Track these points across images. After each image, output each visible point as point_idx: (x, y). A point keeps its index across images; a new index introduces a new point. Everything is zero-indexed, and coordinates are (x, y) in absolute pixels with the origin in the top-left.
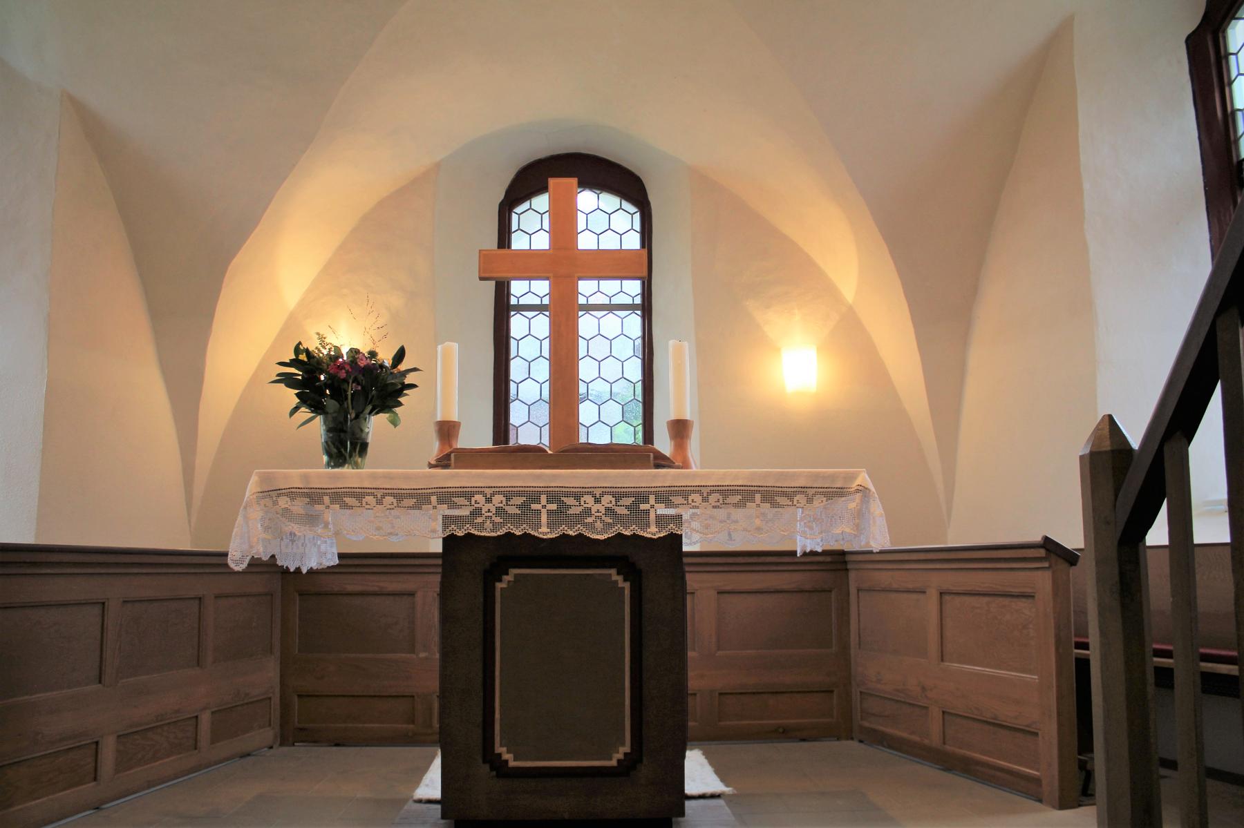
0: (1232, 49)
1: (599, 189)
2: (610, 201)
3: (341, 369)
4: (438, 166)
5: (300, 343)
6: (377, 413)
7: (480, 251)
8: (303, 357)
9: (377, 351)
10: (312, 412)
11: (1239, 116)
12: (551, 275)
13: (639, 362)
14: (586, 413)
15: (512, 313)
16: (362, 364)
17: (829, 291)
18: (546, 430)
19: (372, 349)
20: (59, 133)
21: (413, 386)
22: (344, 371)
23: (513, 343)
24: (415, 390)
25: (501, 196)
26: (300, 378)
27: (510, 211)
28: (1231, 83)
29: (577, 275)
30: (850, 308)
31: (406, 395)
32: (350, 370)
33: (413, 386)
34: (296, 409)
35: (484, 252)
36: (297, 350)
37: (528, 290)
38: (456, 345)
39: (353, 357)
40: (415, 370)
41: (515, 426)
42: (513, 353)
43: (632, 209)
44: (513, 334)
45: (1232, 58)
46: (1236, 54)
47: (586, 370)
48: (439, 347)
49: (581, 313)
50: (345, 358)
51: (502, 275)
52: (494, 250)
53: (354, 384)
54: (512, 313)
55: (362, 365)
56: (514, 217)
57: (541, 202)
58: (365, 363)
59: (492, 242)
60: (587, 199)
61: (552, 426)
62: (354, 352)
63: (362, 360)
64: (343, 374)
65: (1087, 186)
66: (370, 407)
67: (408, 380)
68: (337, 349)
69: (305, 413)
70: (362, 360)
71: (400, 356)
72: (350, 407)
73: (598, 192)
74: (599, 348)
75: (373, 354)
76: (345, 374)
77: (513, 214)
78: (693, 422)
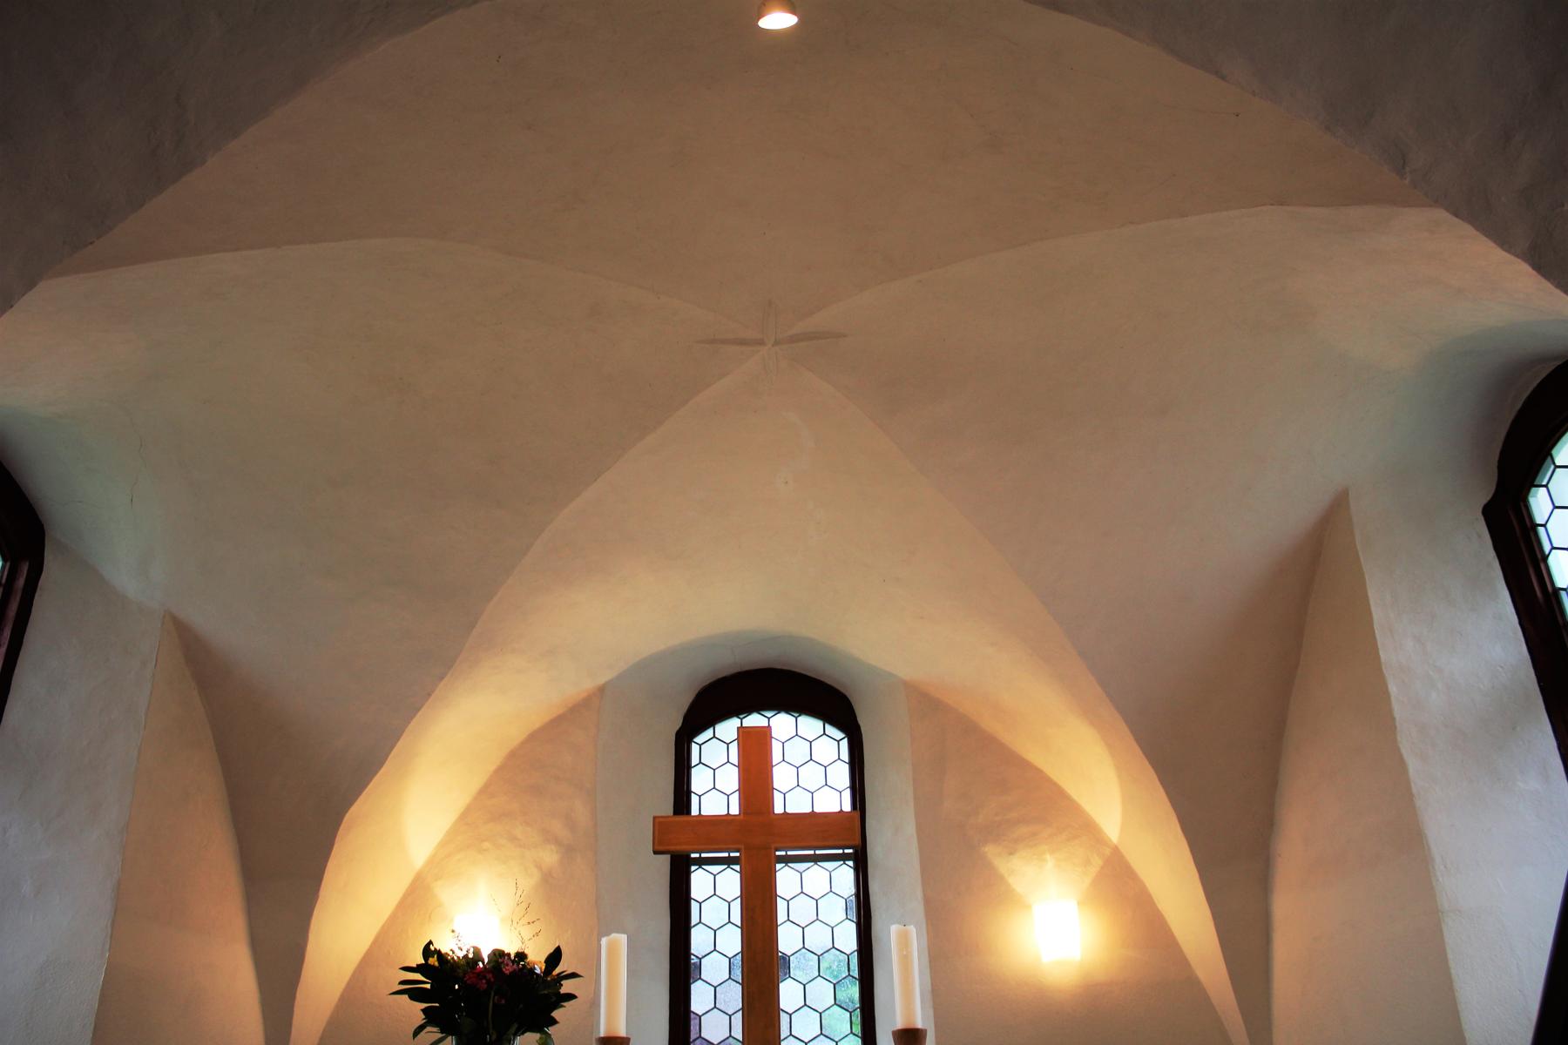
0: (1539, 519)
1: (795, 711)
2: (810, 726)
3: (481, 979)
4: (601, 690)
5: (430, 943)
6: (523, 1034)
7: (655, 818)
8: (433, 961)
9: (526, 952)
10: (442, 1033)
11: (1563, 594)
12: (743, 847)
13: (853, 927)
14: (782, 777)
15: (693, 868)
16: (508, 970)
17: (1087, 829)
18: (735, 799)
19: (520, 951)
20: (156, 661)
21: (570, 997)
22: (484, 981)
23: (694, 907)
24: (573, 1002)
25: (678, 724)
26: (428, 986)
27: (690, 741)
28: (1545, 558)
29: (773, 846)
30: (1116, 850)
31: (564, 1007)
32: (492, 980)
33: (570, 997)
34: (421, 1028)
35: (661, 820)
36: (427, 951)
37: (717, 949)
38: (623, 938)
39: (497, 961)
40: (574, 975)
41: (697, 1015)
42: (694, 919)
43: (838, 734)
44: (694, 788)
45: (1541, 530)
46: (1544, 526)
47: (787, 940)
48: (604, 941)
49: (778, 866)
50: (486, 960)
51: (680, 848)
52: (668, 817)
53: (496, 997)
54: (693, 868)
55: (507, 972)
56: (695, 748)
57: (728, 729)
58: (511, 970)
59: (667, 808)
60: (781, 724)
61: (745, 1013)
62: (498, 955)
63: (507, 965)
64: (483, 985)
65: (1393, 689)
66: (515, 1026)
67: (567, 987)
68: (477, 952)
69: (432, 1033)
70: (507, 965)
71: (555, 957)
72: (491, 1026)
73: (796, 715)
74: (802, 910)
75: (521, 956)
76: (486, 986)
77: (693, 744)
78: (926, 1030)
